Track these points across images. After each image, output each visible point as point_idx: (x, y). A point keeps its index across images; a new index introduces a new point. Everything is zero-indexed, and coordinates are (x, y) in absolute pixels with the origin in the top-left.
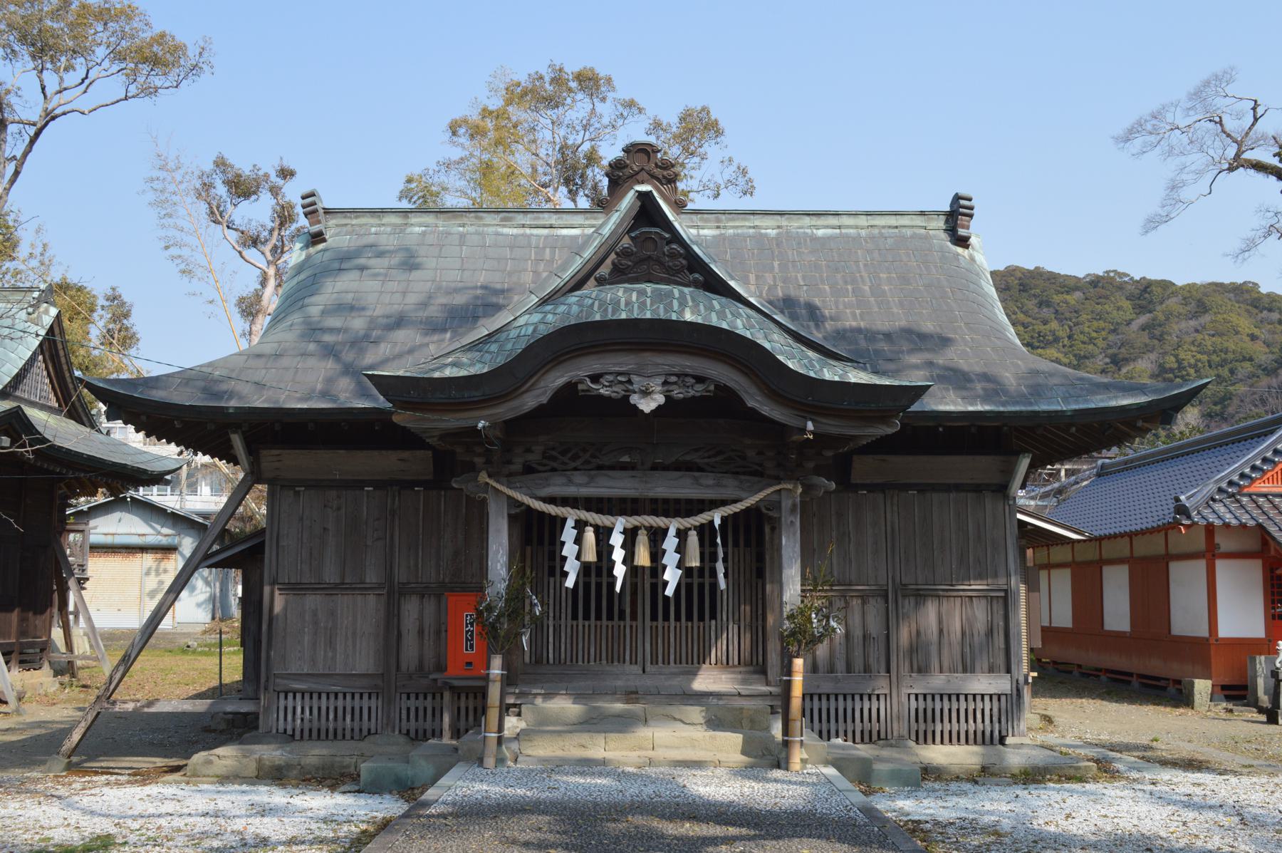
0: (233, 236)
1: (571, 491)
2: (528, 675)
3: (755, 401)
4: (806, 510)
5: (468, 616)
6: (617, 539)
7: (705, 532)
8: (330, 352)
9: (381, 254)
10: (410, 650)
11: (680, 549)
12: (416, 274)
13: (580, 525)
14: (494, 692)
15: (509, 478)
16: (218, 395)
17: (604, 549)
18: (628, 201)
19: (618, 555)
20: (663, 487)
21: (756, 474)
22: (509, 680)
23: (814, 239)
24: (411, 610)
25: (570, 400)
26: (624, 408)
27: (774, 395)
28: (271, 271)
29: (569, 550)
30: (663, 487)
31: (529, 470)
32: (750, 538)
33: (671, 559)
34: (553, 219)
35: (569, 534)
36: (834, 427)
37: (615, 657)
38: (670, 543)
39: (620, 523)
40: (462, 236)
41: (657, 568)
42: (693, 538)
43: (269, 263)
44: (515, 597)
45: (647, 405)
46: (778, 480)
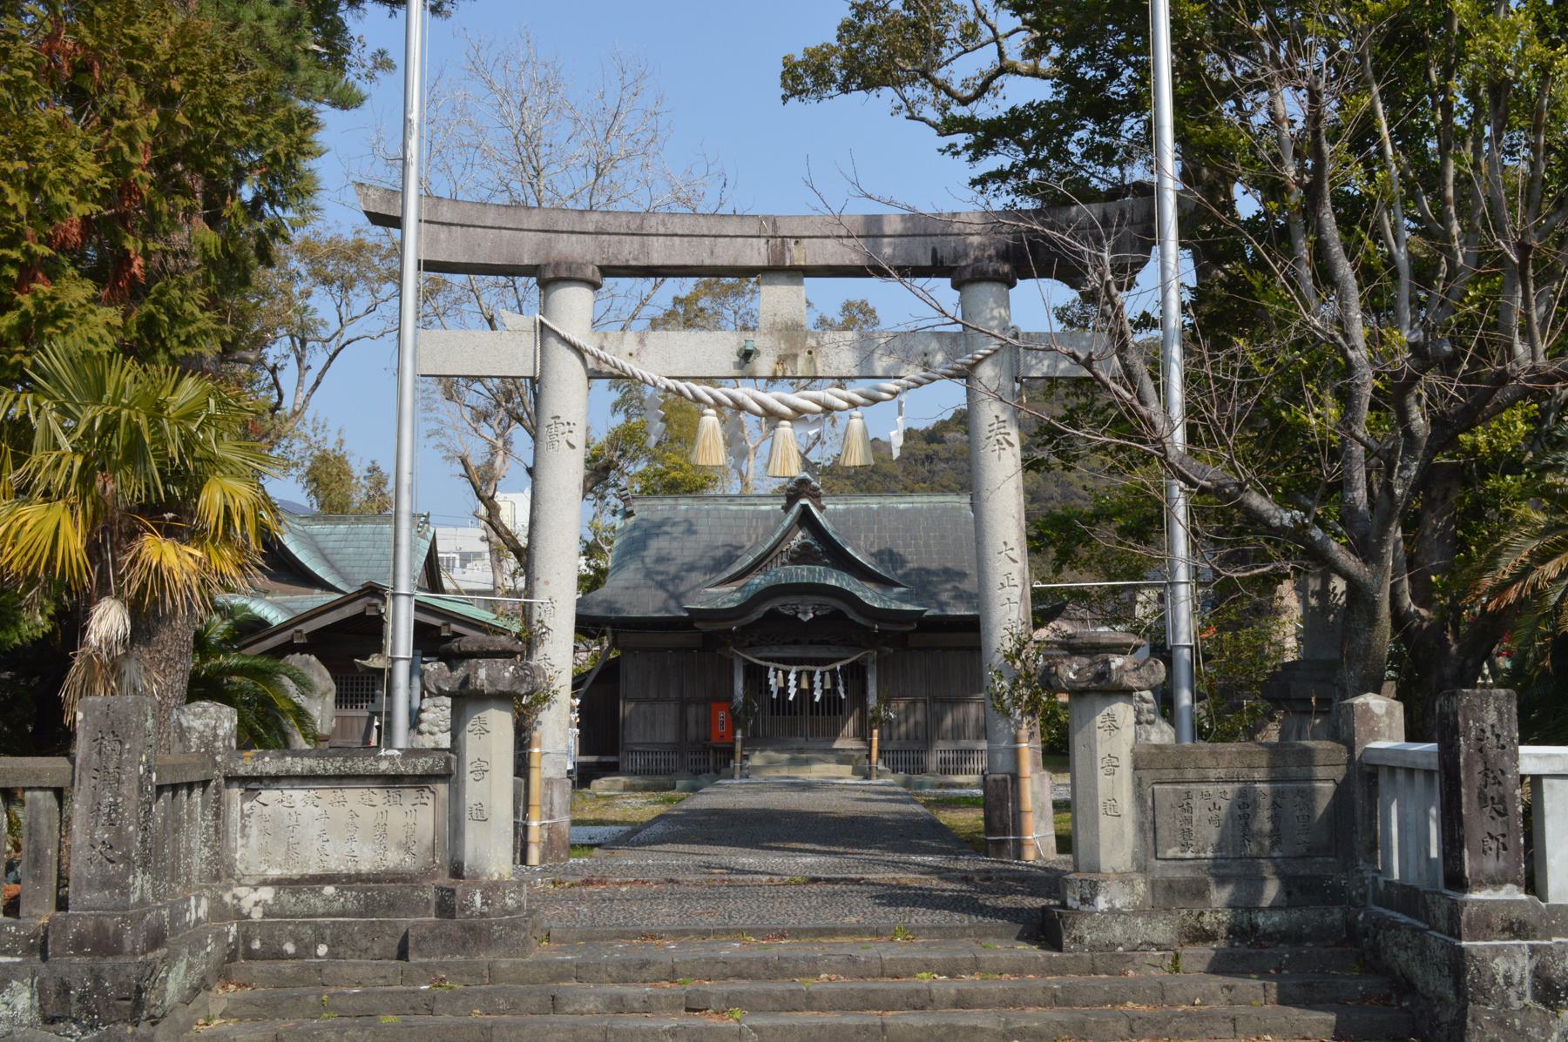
0: (467, 413)
1: (771, 655)
2: (755, 741)
3: (852, 616)
4: (882, 663)
5: (722, 714)
6: (792, 677)
7: (833, 673)
8: (661, 585)
9: (674, 524)
10: (692, 731)
11: (822, 680)
12: (693, 538)
13: (776, 670)
14: (738, 746)
15: (743, 649)
16: (617, 611)
17: (786, 681)
18: (796, 508)
19: (792, 683)
20: (813, 653)
21: (858, 646)
22: (744, 742)
23: (898, 511)
24: (692, 711)
25: (773, 615)
26: (795, 618)
27: (859, 613)
28: (500, 443)
29: (772, 681)
30: (813, 653)
31: (751, 645)
32: (855, 675)
33: (817, 685)
34: (756, 501)
35: (771, 674)
36: (887, 627)
37: (792, 734)
38: (817, 678)
39: (794, 669)
40: (708, 511)
41: (812, 689)
42: (827, 676)
43: (498, 436)
44: (746, 702)
45: (806, 619)
46: (865, 648)
